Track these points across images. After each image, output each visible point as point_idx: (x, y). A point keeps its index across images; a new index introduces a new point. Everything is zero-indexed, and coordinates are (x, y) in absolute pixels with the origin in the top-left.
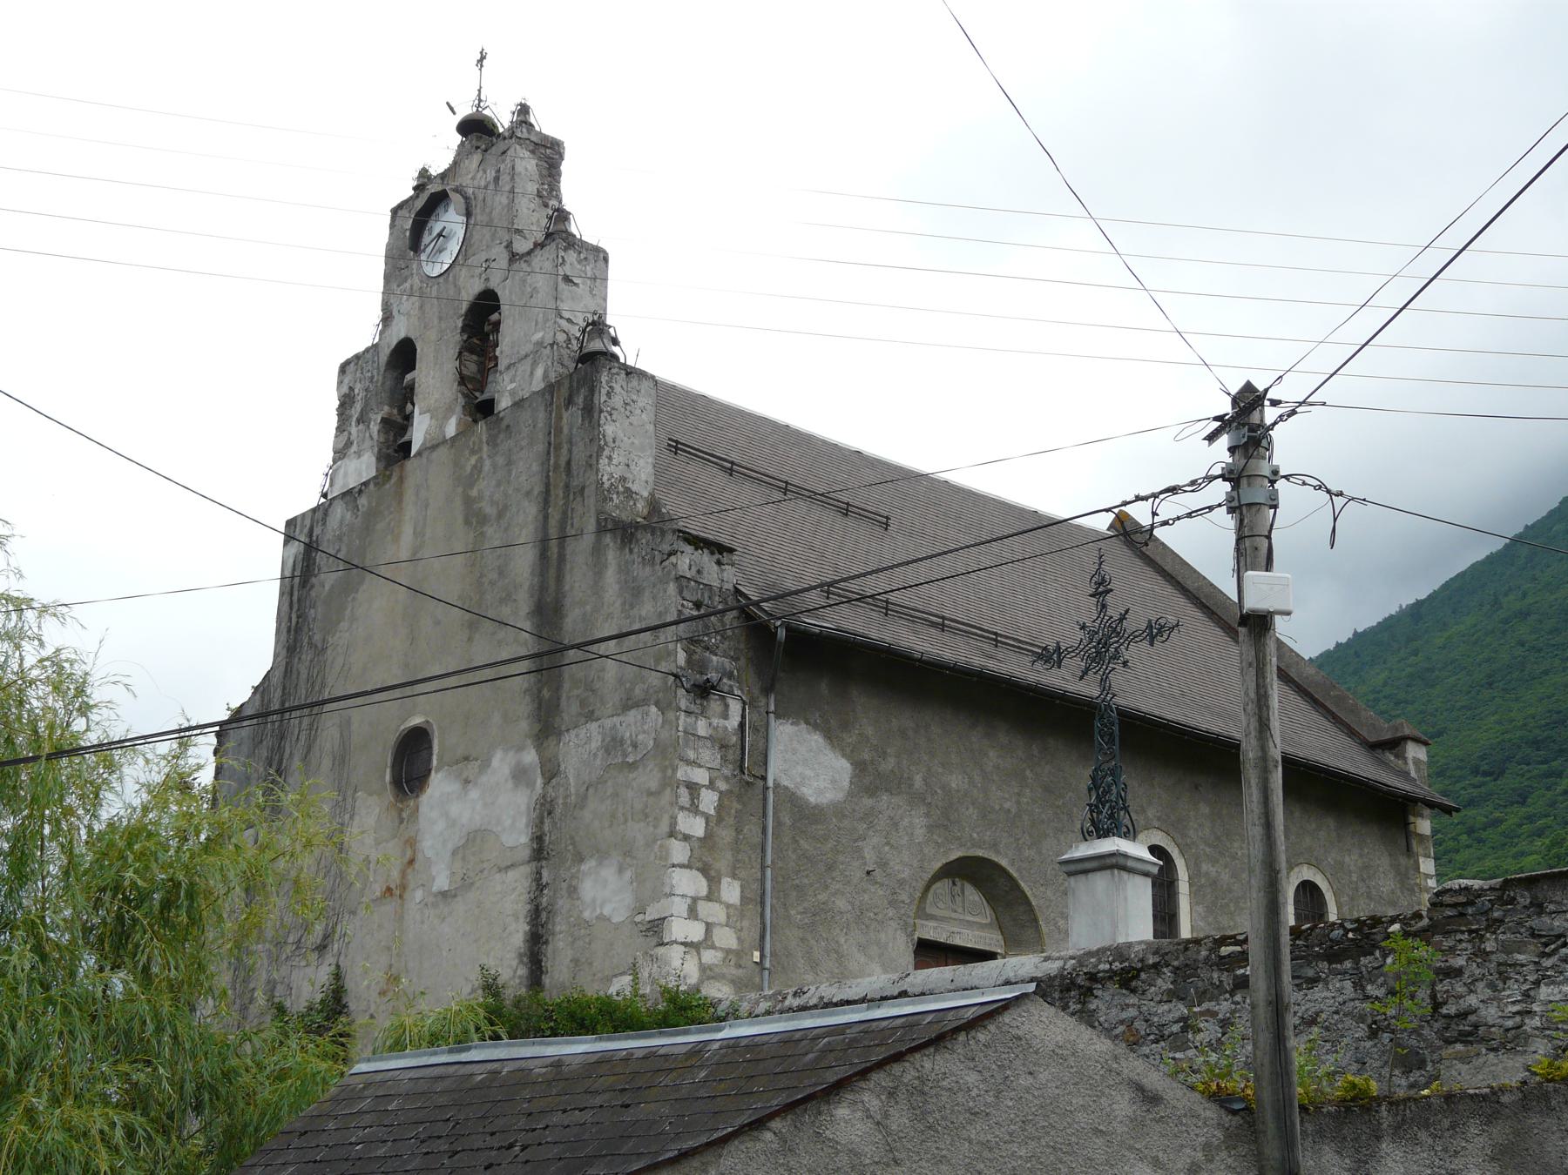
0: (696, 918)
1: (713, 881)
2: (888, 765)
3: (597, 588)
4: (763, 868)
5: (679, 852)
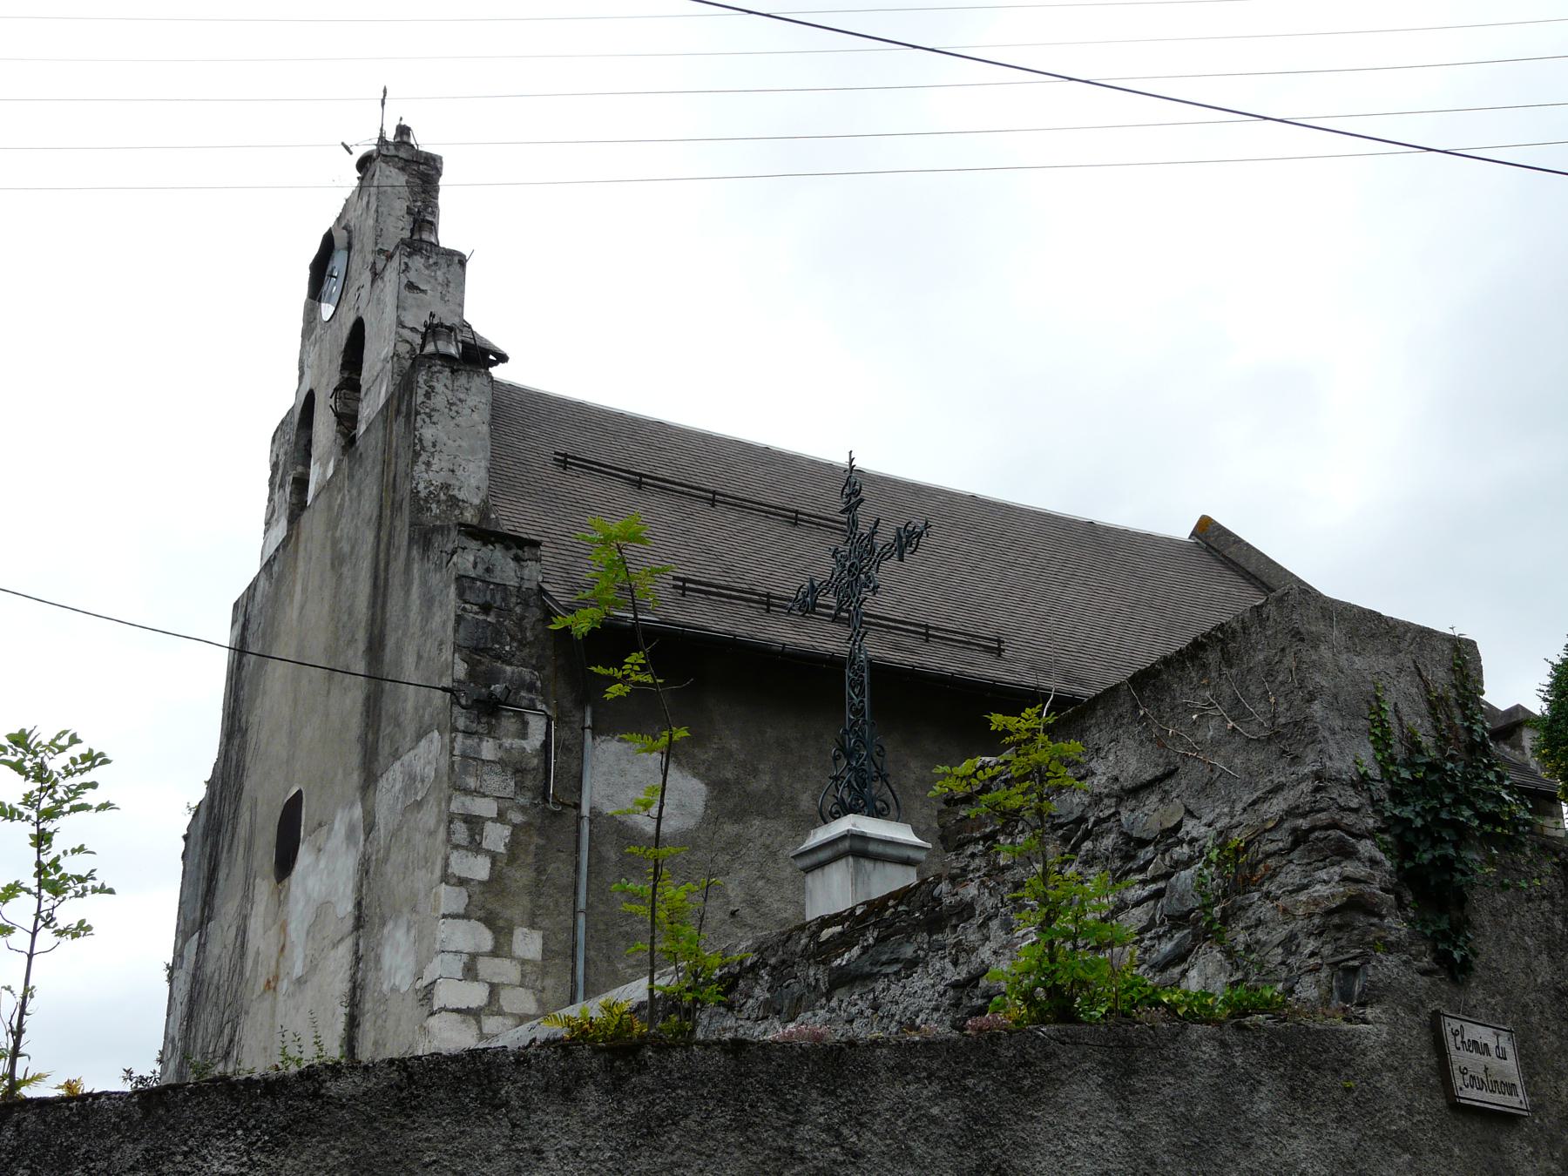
0: (475, 978)
1: (501, 932)
2: (762, 783)
3: (406, 608)
4: (575, 913)
5: (451, 898)
